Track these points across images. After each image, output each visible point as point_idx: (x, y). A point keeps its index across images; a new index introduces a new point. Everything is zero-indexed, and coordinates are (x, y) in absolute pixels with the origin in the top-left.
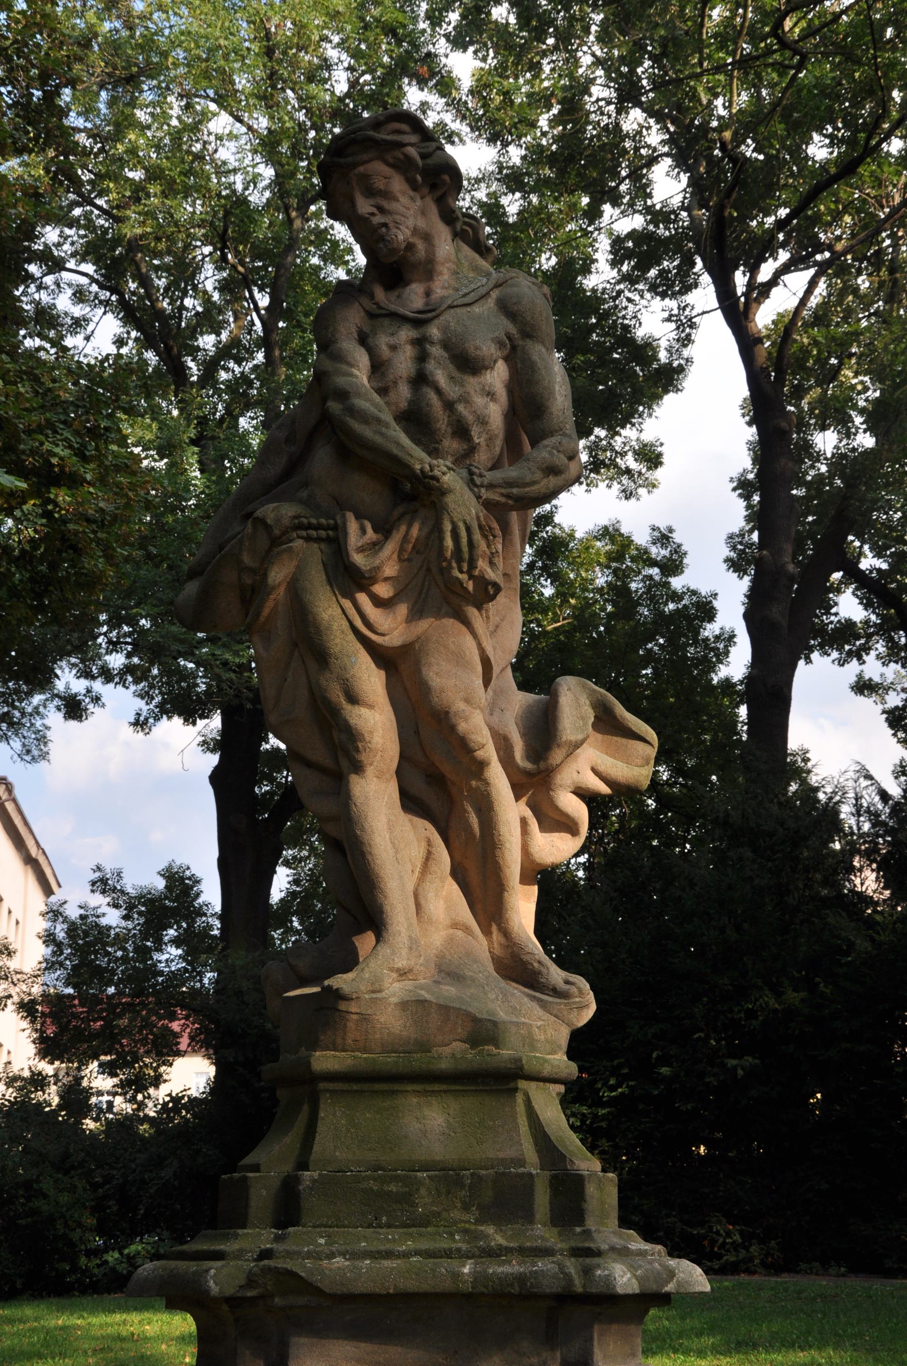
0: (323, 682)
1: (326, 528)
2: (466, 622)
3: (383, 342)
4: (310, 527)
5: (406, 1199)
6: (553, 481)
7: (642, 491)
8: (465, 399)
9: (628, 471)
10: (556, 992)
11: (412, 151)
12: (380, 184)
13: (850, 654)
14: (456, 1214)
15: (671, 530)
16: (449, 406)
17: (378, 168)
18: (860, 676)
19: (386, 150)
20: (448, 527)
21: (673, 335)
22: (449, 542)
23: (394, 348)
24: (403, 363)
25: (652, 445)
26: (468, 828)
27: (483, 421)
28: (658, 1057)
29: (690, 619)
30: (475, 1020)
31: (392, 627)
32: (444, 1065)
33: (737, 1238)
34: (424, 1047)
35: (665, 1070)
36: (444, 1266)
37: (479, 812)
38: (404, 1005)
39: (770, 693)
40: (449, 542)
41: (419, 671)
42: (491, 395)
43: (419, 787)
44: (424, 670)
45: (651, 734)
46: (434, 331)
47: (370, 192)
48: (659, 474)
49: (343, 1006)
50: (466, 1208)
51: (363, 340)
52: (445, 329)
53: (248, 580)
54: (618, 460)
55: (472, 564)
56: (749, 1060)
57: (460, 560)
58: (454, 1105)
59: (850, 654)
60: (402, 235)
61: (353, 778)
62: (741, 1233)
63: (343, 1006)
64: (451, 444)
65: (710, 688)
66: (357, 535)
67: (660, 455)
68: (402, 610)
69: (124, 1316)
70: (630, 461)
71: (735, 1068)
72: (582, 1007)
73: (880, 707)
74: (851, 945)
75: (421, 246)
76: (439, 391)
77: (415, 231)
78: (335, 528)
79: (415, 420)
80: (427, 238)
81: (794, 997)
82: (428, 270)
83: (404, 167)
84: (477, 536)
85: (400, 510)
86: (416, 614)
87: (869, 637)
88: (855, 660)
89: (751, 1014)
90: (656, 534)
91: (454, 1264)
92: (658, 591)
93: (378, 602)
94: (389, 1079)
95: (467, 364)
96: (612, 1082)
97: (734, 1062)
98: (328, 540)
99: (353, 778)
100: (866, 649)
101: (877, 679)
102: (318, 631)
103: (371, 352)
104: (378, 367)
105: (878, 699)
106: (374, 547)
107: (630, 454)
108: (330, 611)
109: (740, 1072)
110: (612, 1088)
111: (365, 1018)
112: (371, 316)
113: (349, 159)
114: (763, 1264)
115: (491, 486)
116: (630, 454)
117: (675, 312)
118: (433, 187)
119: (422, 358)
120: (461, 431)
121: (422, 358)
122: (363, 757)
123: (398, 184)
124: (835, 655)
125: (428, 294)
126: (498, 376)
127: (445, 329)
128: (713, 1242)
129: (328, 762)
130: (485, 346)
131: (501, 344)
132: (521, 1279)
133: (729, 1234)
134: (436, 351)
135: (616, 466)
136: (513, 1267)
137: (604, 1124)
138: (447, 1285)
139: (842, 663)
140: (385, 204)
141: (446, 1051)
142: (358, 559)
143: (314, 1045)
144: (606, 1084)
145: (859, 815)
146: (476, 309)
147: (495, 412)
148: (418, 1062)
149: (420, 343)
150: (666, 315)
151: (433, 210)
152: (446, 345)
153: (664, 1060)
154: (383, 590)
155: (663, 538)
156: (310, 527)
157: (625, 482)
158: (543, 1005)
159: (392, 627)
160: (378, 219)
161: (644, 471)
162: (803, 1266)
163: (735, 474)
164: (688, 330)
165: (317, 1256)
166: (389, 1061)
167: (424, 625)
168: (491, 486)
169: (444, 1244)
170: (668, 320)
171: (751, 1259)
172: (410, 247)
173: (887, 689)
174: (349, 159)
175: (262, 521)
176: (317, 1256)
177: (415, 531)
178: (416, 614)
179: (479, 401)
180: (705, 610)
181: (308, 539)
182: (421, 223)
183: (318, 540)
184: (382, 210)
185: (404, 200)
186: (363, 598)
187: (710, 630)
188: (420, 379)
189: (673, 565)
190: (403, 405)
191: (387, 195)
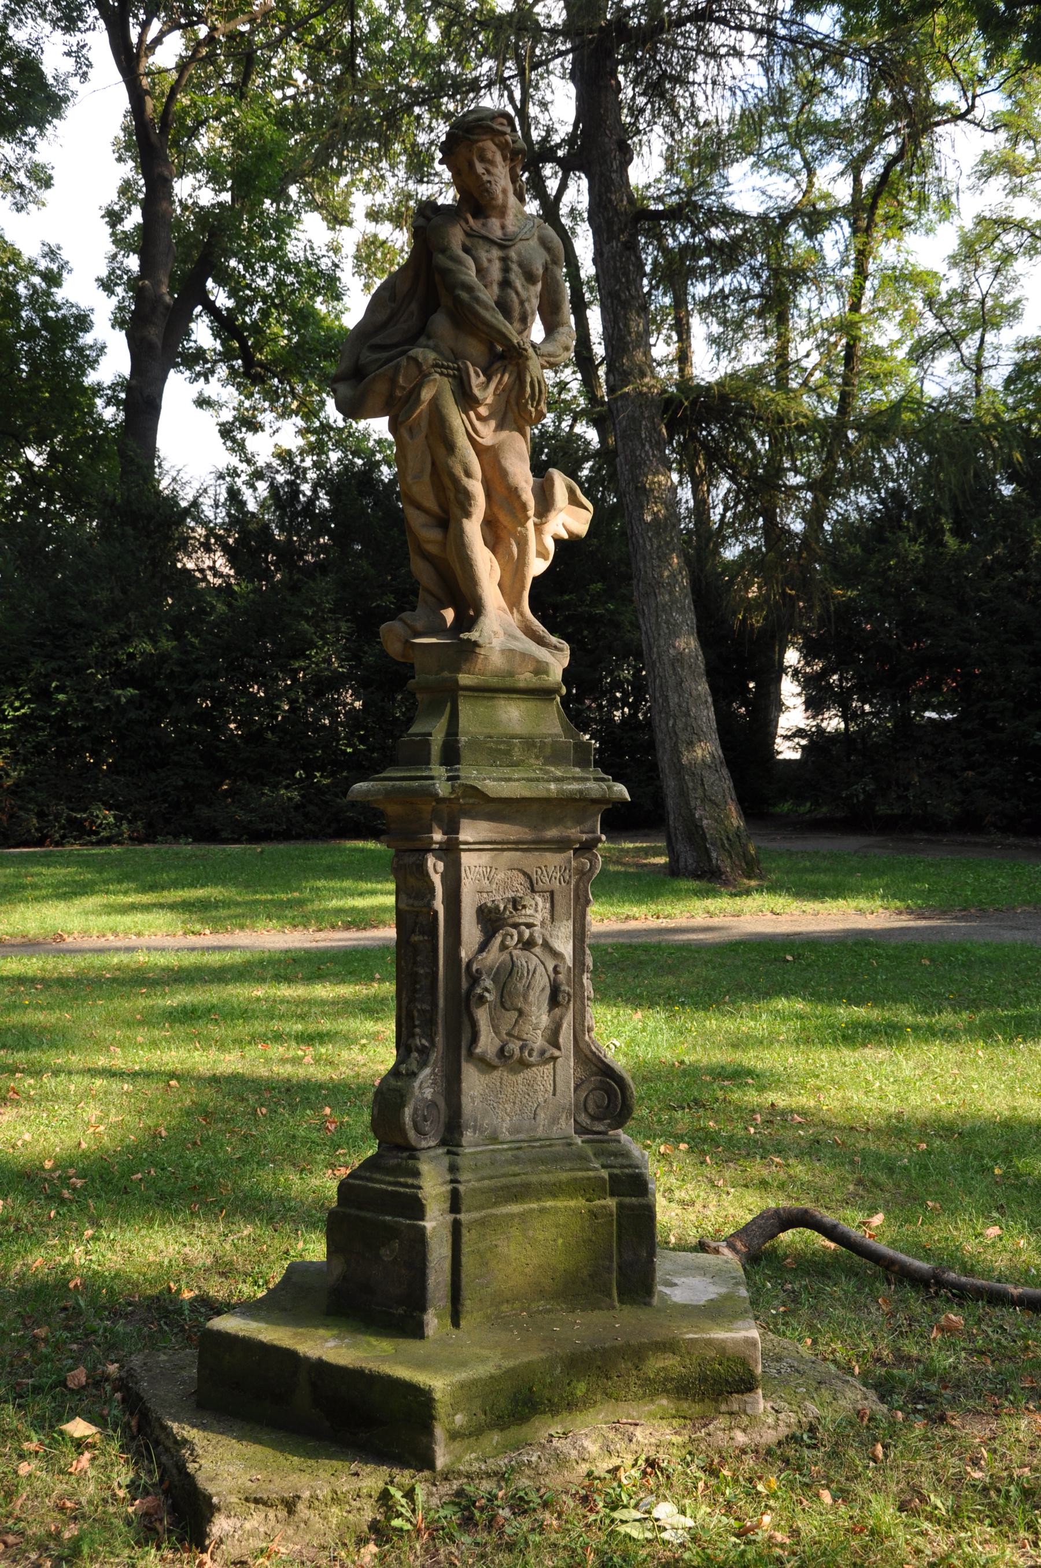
0: (450, 462)
1: (453, 369)
4: (443, 366)
5: (508, 753)
7: (31, 206)
9: (21, 186)
10: (556, 648)
12: (489, 155)
13: (199, 374)
14: (532, 761)
15: (59, 248)
16: (522, 303)
18: (201, 394)
20: (528, 380)
22: (528, 389)
24: (495, 272)
25: (44, 167)
26: (511, 554)
28: (56, 687)
29: (68, 326)
31: (487, 434)
32: (522, 685)
33: (112, 819)
34: (511, 674)
35: (61, 697)
36: (542, 785)
37: (518, 545)
38: (503, 651)
39: (142, 400)
40: (528, 389)
41: (499, 462)
44: (503, 461)
45: (590, 507)
47: (483, 159)
48: (45, 195)
49: (478, 650)
50: (537, 758)
51: (466, 250)
52: (519, 254)
54: (12, 174)
55: (538, 404)
56: (131, 691)
57: (533, 400)
58: (523, 705)
59: (199, 374)
61: (465, 521)
62: (115, 816)
63: (478, 650)
65: (83, 390)
66: (476, 380)
67: (51, 178)
68: (493, 424)
70: (21, 177)
71: (119, 696)
73: (215, 420)
74: (213, 607)
76: (517, 293)
78: (459, 369)
81: (167, 644)
86: (500, 427)
87: (215, 362)
88: (202, 379)
89: (131, 656)
90: (46, 249)
91: (546, 785)
92: (41, 301)
93: (480, 418)
94: (488, 692)
96: (17, 704)
97: (119, 692)
98: (454, 377)
99: (465, 521)
100: (212, 372)
101: (214, 397)
102: (452, 433)
103: (476, 260)
104: (480, 271)
105: (214, 414)
106: (485, 386)
107: (22, 171)
108: (456, 419)
109: (123, 700)
110: (17, 709)
111: (486, 658)
113: (476, 137)
114: (131, 838)
116: (22, 171)
117: (74, 49)
118: (512, 160)
119: (506, 270)
122: (472, 509)
124: (188, 374)
127: (519, 254)
128: (93, 822)
132: (581, 791)
133: (105, 818)
134: (515, 267)
135: (10, 180)
136: (575, 786)
137: (8, 737)
138: (543, 794)
139: (193, 380)
140: (490, 168)
141: (522, 677)
143: (458, 670)
144: (11, 705)
145: (217, 507)
148: (508, 682)
149: (505, 260)
150: (66, 49)
152: (521, 265)
153: (60, 689)
154: (483, 411)
155: (52, 253)
156: (443, 366)
157: (18, 196)
158: (553, 655)
159: (487, 434)
160: (486, 178)
161: (35, 188)
162: (160, 838)
163: (105, 205)
164: (85, 68)
166: (494, 682)
167: (504, 434)
169: (533, 775)
170: (68, 54)
171: (121, 835)
173: (221, 406)
174: (476, 137)
175: (415, 359)
177: (506, 378)
178: (500, 427)
180: (83, 322)
181: (441, 374)
183: (448, 376)
184: (488, 172)
187: (87, 339)
189: (53, 279)
191: (492, 163)
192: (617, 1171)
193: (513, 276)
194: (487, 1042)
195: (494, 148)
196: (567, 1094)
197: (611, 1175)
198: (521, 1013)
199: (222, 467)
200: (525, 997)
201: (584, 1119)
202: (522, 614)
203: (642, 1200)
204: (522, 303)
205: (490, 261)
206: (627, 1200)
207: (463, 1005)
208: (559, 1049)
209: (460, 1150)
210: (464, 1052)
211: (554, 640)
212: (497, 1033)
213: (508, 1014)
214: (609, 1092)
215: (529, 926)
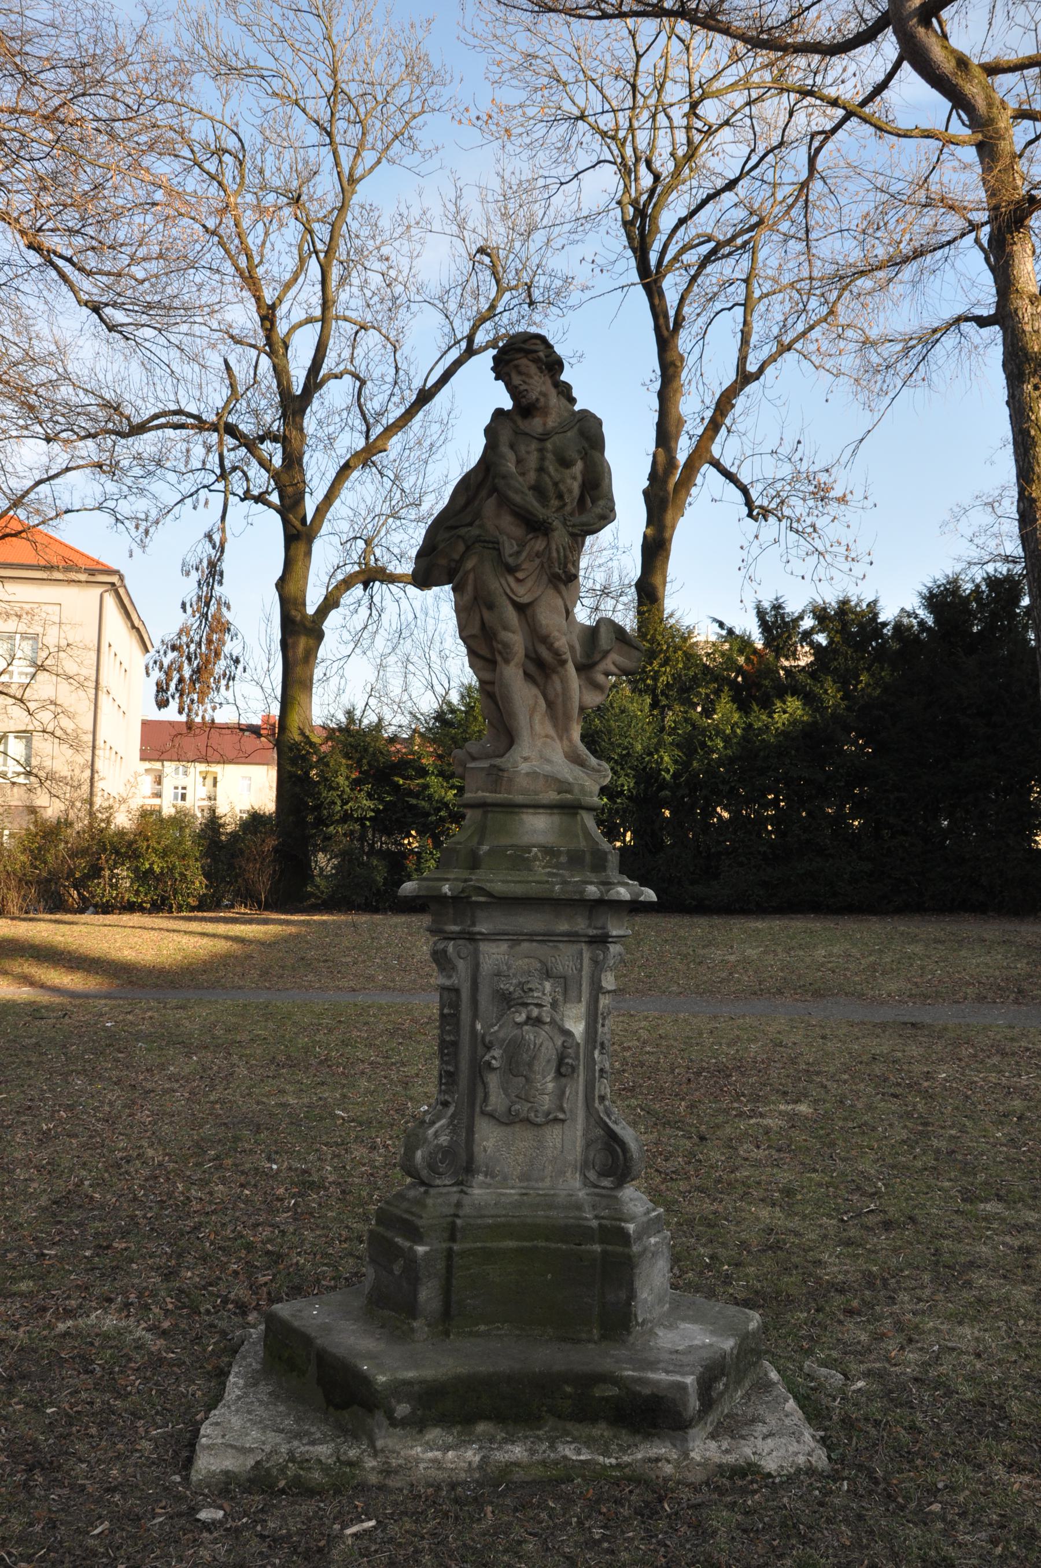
2: (559, 592)
3: (523, 449)
6: (603, 522)
8: (563, 481)
11: (541, 354)
16: (556, 484)
17: (524, 361)
19: (527, 352)
20: (554, 547)
21: (713, 638)
23: (528, 453)
24: (533, 460)
27: (570, 491)
30: (560, 781)
32: (545, 802)
42: (574, 478)
43: (532, 669)
46: (549, 445)
51: (512, 446)
53: (453, 565)
55: (565, 566)
60: (533, 395)
64: (555, 503)
69: (355, 918)
72: (605, 776)
75: (542, 400)
77: (541, 393)
79: (538, 489)
80: (545, 395)
82: (545, 412)
83: (536, 361)
84: (568, 553)
85: (530, 536)
95: (565, 463)
104: (519, 461)
112: (516, 433)
115: (574, 526)
119: (542, 459)
120: (560, 496)
121: (542, 459)
123: (533, 369)
125: (545, 424)
126: (579, 467)
129: (489, 656)
130: (572, 453)
131: (579, 452)
134: (550, 456)
142: (510, 561)
146: (569, 434)
147: (576, 487)
149: (541, 450)
151: (549, 382)
153: (862, 792)
160: (522, 388)
165: (491, 881)
168: (574, 526)
172: (537, 400)
176: (491, 881)
179: (569, 481)
182: (544, 389)
185: (536, 378)
186: (511, 580)
188: (541, 469)
190: (533, 482)
192: (604, 1222)
193: (547, 463)
194: (497, 1100)
195: (530, 363)
196: (576, 1149)
197: (600, 1225)
198: (528, 1080)
199: (909, 608)
200: (530, 1065)
201: (592, 1175)
202: (570, 740)
203: (626, 1250)
204: (556, 484)
205: (528, 453)
206: (610, 1248)
207: (480, 1070)
208: (564, 1112)
209: (469, 1190)
210: (478, 1109)
211: (593, 761)
212: (507, 1095)
213: (516, 1079)
214: (613, 1153)
215: (539, 1006)
